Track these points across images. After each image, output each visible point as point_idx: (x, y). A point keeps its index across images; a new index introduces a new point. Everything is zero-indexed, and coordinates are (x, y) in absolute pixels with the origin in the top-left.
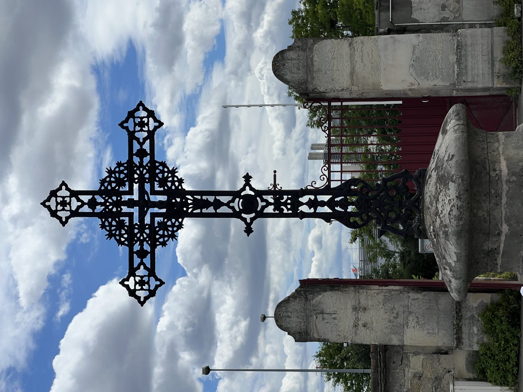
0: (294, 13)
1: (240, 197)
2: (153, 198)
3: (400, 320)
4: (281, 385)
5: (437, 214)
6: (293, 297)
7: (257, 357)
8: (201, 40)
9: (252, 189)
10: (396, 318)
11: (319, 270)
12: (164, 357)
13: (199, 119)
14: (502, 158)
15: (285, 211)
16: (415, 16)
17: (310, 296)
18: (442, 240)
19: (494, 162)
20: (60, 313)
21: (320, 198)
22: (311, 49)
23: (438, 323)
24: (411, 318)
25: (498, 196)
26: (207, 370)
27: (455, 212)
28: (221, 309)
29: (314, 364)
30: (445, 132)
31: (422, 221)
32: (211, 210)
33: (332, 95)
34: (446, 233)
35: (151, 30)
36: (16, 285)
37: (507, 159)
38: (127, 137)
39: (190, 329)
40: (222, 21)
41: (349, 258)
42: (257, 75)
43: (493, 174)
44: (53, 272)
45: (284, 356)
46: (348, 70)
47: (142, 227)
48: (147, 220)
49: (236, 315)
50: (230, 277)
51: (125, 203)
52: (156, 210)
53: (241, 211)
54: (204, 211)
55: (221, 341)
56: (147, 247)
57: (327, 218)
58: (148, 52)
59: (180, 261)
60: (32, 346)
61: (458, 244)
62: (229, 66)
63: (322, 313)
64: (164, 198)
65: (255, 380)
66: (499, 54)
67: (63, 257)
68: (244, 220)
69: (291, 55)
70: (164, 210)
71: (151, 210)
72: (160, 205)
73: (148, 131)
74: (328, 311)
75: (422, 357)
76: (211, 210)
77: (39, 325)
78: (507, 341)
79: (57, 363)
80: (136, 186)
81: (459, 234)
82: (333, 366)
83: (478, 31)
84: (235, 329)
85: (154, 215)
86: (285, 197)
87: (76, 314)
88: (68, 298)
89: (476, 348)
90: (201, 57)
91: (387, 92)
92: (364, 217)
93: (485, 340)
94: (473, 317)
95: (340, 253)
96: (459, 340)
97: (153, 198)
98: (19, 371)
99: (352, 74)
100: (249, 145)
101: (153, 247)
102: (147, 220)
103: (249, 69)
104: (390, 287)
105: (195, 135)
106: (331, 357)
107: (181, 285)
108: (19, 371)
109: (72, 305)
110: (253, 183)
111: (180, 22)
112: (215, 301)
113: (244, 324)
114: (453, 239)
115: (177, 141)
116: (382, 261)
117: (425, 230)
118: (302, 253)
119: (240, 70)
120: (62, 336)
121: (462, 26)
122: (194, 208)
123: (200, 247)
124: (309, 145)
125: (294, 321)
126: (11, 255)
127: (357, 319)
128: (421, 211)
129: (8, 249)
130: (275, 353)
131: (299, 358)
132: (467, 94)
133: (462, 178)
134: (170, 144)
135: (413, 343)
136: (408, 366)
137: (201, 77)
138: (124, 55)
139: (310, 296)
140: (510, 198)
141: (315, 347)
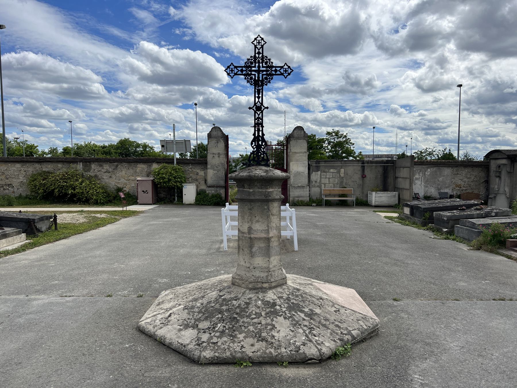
0: (315, 135)
1: (261, 105)
2: (261, 75)
3: (216, 168)
4: (192, 131)
5: (256, 170)
6: (223, 133)
7: (201, 123)
8: (308, 104)
9: (264, 109)
10: (216, 167)
11: (231, 144)
12: (201, 90)
13: (281, 104)
14: (273, 190)
15: (256, 121)
16: (314, 173)
17: (223, 138)
18: (247, 171)
19: (272, 187)
20: (216, 53)
21: (261, 132)
22: (304, 139)
23: (215, 180)
24: (216, 172)
25: (262, 188)
26: (196, 104)
27: (257, 175)
28: (217, 111)
29: (199, 142)
30: (282, 172)
31: (253, 165)
32: (257, 95)
33: (289, 146)
34: (250, 172)
35: (312, 87)
36: (226, 37)
37: (273, 191)
38: (282, 66)
39: (210, 100)
40: (314, 111)
41: (235, 154)
42: (295, 124)
43: (268, 187)
44: (230, 51)
45: (201, 132)
46: (297, 151)
47: (251, 71)
48: (253, 73)
49: (216, 116)
50: (228, 114)
51: (259, 65)
52: (257, 76)
53: (256, 106)
54: (257, 93)
55: (206, 111)
56: (244, 72)
57: (254, 135)
58: (305, 86)
59: (234, 96)
60: (204, 43)
61: (246, 176)
62: (298, 114)
63: (217, 143)
64: (261, 79)
65: (193, 122)
66: (300, 199)
67: (235, 54)
68: (253, 107)
69: (303, 132)
70: (257, 79)
71: (257, 74)
72: (259, 77)
73: (283, 73)
74: (218, 144)
75: (204, 175)
76: (257, 95)
77: (212, 45)
78: (210, 201)
79: (199, 52)
80: (265, 69)
81: (249, 176)
82: (199, 148)
83: (308, 193)
84: (211, 116)
85: (255, 75)
86: (261, 121)
87: (215, 59)
88: (221, 56)
89: (207, 192)
90: (302, 104)
91: (289, 164)
92: (254, 147)
93: (210, 195)
94: (217, 191)
95: (236, 151)
96: (210, 187)
97: (261, 75)
98: (195, 38)
99: (296, 153)
100: (272, 121)
101: (255, 56)
102: (253, 73)
103: (297, 121)
104: (226, 165)
105: (276, 102)
106: (202, 147)
107: (226, 97)
108: (195, 38)
109: (219, 57)
110: (266, 109)
111: (314, 97)
112: (220, 109)
113: (212, 119)
114: (248, 174)
115: (274, 96)
116: (234, 164)
117: (250, 166)
118: (236, 139)
119: (297, 118)
120: (208, 54)
121: (310, 188)
122: (257, 89)
123: (238, 104)
124: (271, 141)
125: (214, 133)
126: (236, 36)
127: (215, 154)
128: (256, 165)
129: (238, 35)
130: (203, 129)
131: (201, 137)
132: (288, 189)
133: (267, 177)
134: (273, 93)
135: (208, 172)
136: (201, 171)
137: (296, 104)
138: (304, 77)
139: (223, 138)
140: (261, 192)
141: (205, 142)
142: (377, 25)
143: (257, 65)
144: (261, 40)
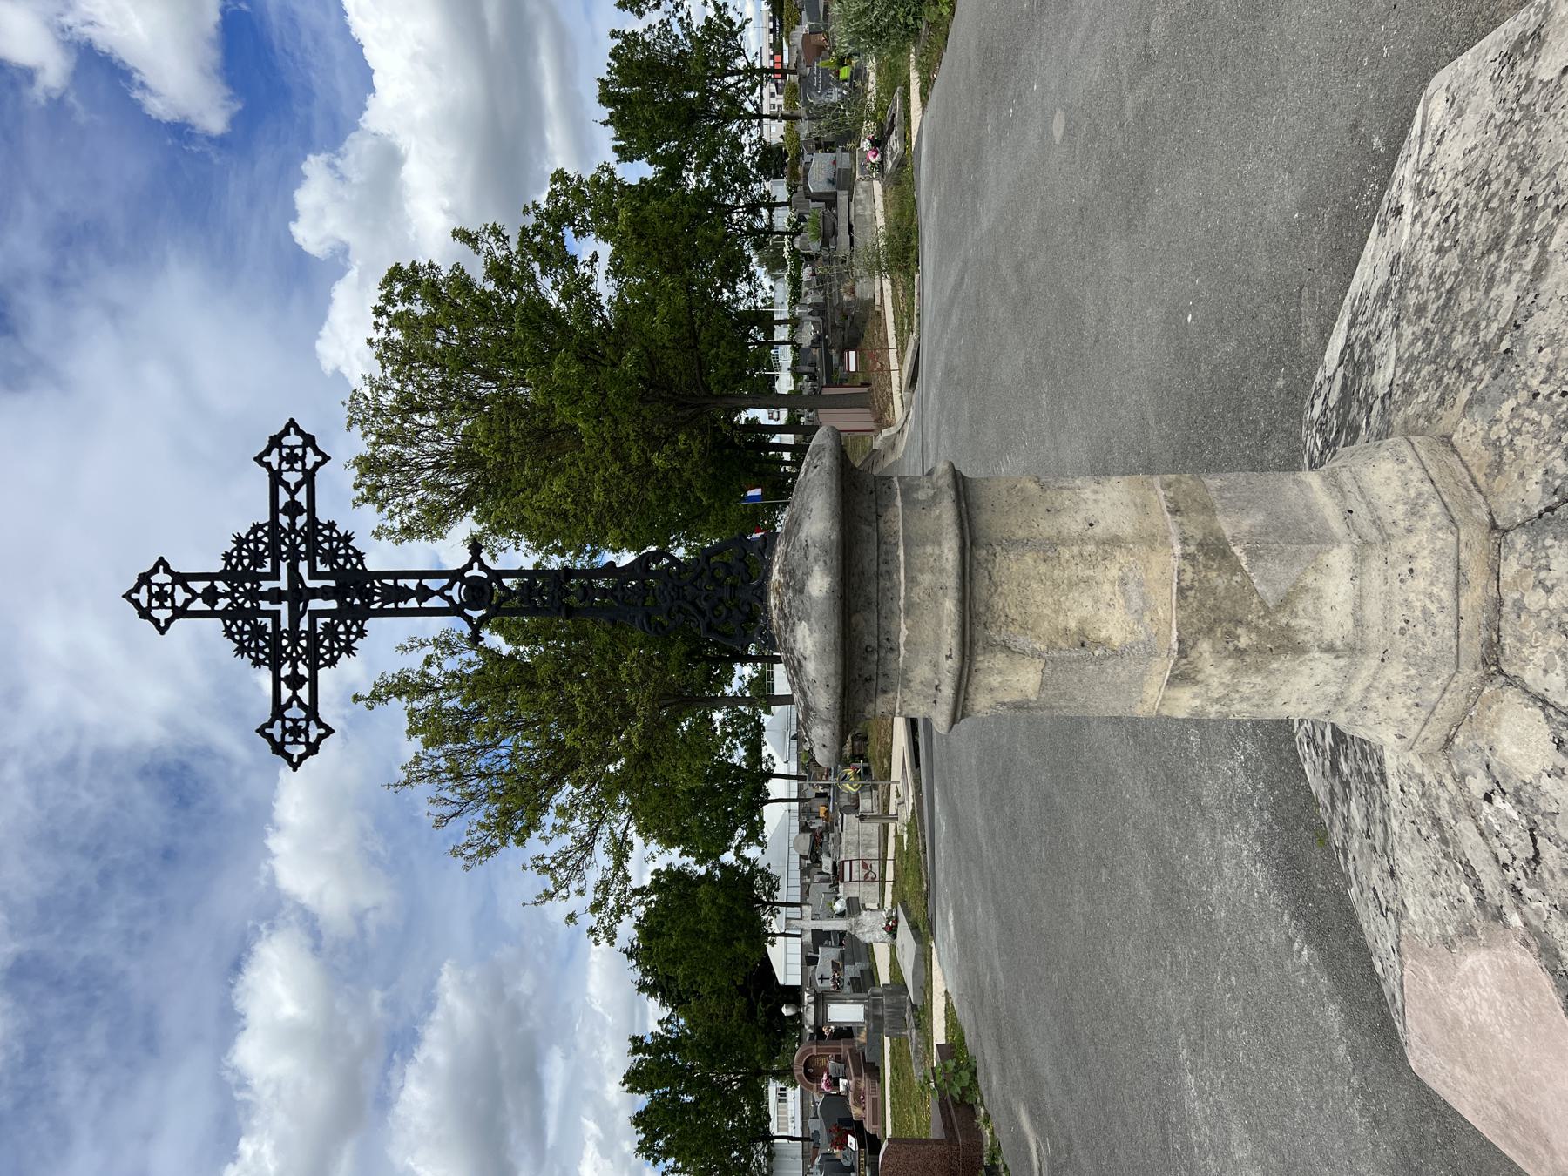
143: (265, 605)
144: (150, 584)
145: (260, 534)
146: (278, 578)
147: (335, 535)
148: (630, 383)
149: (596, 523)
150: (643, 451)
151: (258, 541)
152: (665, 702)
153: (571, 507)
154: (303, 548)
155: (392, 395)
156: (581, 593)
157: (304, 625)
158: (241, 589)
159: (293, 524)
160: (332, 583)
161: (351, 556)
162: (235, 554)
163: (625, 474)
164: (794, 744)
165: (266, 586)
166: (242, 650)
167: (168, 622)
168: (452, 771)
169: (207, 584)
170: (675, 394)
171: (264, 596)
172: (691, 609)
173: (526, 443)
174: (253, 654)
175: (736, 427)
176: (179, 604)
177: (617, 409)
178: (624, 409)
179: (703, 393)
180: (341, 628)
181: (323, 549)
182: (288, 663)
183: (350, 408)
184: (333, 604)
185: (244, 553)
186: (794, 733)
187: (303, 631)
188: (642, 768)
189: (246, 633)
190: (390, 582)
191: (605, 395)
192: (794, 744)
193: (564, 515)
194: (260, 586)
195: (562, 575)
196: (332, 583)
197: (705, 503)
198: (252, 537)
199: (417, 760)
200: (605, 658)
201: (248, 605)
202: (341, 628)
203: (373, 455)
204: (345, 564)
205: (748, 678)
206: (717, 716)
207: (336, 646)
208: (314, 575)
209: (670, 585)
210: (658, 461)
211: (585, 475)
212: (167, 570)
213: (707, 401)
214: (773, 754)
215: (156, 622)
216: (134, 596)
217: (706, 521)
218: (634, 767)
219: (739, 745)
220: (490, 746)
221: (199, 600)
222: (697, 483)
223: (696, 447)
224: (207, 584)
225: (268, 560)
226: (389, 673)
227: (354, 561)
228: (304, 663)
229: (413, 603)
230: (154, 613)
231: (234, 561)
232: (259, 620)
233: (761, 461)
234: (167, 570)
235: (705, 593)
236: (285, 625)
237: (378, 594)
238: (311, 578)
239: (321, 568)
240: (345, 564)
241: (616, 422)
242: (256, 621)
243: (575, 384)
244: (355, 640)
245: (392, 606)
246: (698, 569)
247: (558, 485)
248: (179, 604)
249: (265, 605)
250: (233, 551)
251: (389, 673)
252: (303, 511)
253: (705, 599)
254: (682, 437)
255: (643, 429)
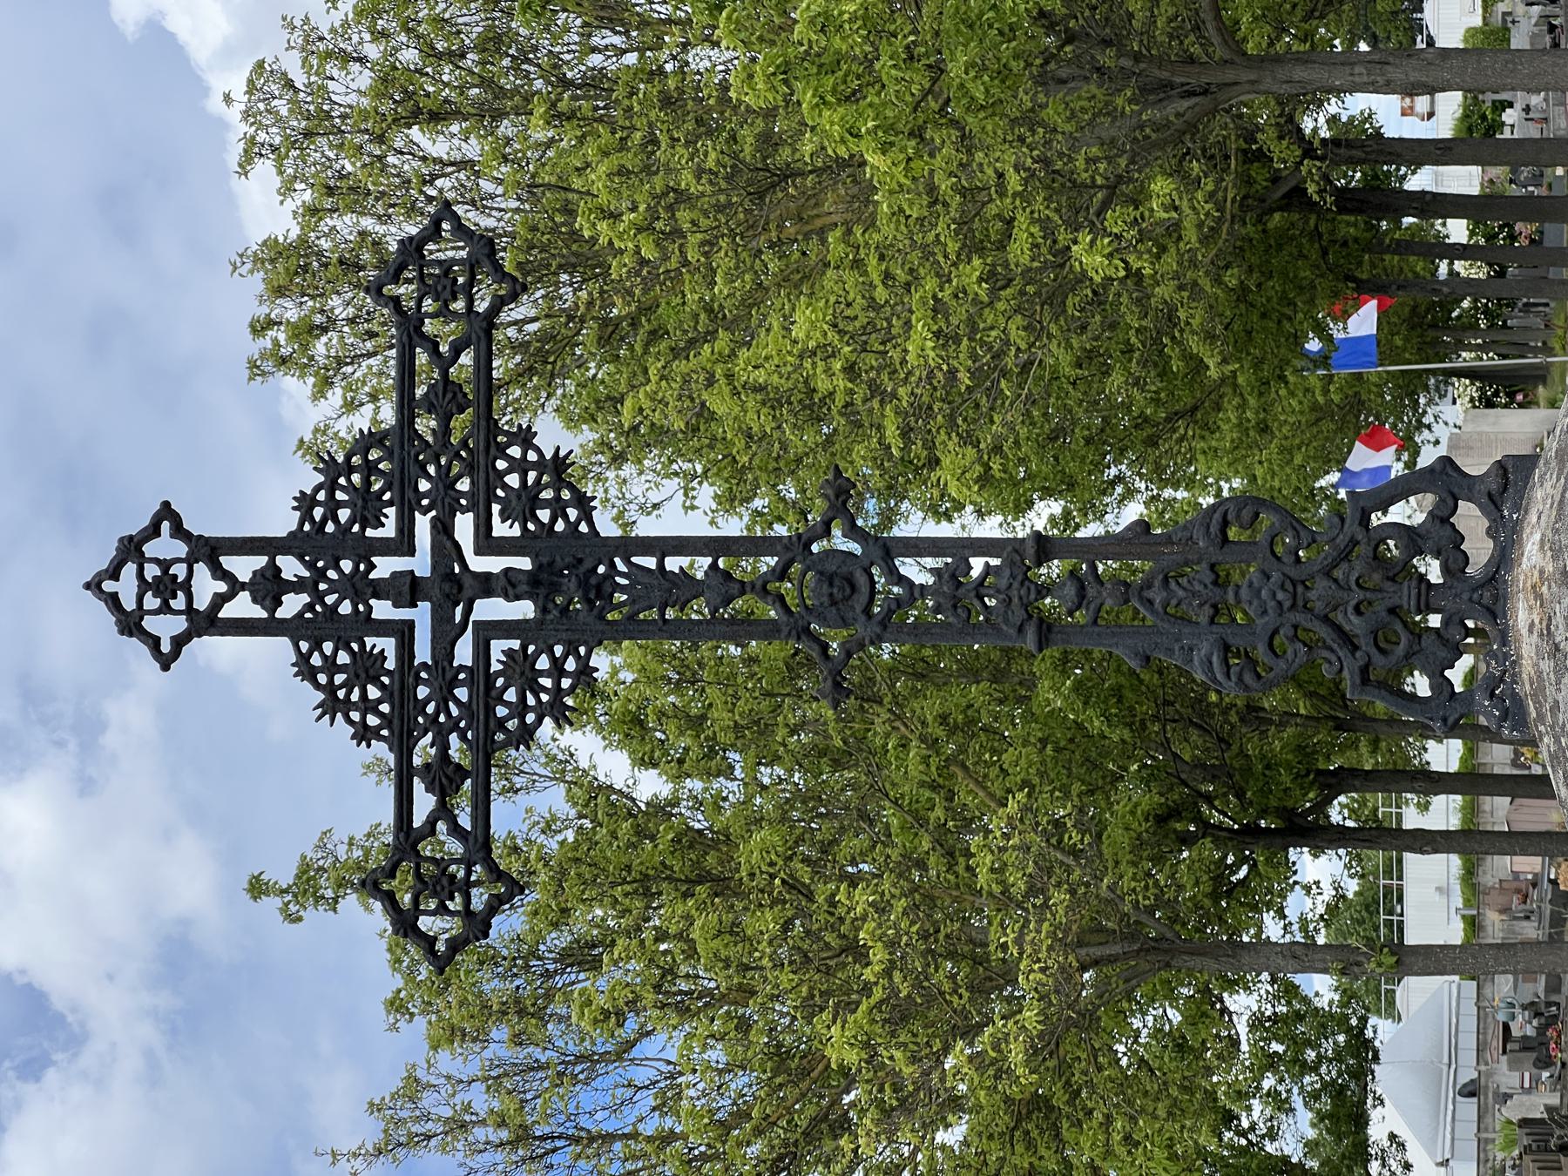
142: (265, 243)
143: (382, 609)
144: (141, 560)
145: (374, 455)
146: (411, 552)
147: (532, 456)
148: (1009, 33)
149: (906, 433)
150: (1048, 230)
151: (370, 469)
152: (1097, 952)
153: (841, 383)
154: (464, 485)
155: (363, 78)
156: (1070, 591)
157: (464, 653)
158: (332, 574)
159: (444, 431)
160: (524, 563)
161: (567, 504)
162: (321, 496)
163: (994, 292)
164: (1469, 1107)
165: (385, 566)
166: (332, 706)
167: (179, 642)
168: (502, 1124)
169: (260, 561)
170: (1137, 57)
171: (379, 590)
172: (1324, 632)
173: (720, 208)
174: (355, 716)
175: (1308, 148)
176: (201, 603)
177: (973, 106)
178: (992, 107)
179: (1220, 52)
180: (543, 663)
181: (505, 487)
182: (430, 736)
183: (246, 114)
184: (524, 609)
185: (340, 496)
186: (1468, 1075)
187: (462, 668)
188: (1030, 1145)
189: (341, 669)
190: (650, 562)
191: (937, 70)
192: (1469, 1107)
193: (813, 407)
194: (372, 567)
195: (1030, 550)
196: (524, 563)
197: (1213, 373)
198: (356, 460)
199: (413, 1087)
200: (922, 821)
201: (345, 608)
202: (543, 663)
203: (303, 240)
204: (553, 520)
205: (1328, 894)
206: (1242, 1004)
207: (531, 701)
208: (487, 543)
209: (1276, 576)
210: (1090, 258)
211: (881, 294)
212: (179, 531)
213: (1229, 75)
214: (1404, 1134)
215: (154, 642)
216: (108, 586)
217: (1210, 429)
218: (1008, 1137)
219: (1297, 1101)
220: (605, 1057)
221: (244, 596)
222: (1193, 316)
223: (1196, 211)
224: (260, 561)
225: (391, 511)
226: (341, 835)
227: (573, 513)
228: (463, 738)
229: (698, 610)
230: (149, 623)
231: (318, 513)
232: (369, 641)
233: (1376, 245)
234: (179, 531)
235: (1358, 595)
236: (423, 652)
237: (623, 589)
238: (478, 552)
239: (501, 529)
240: (553, 520)
241: (966, 142)
242: (363, 645)
243: (854, 42)
244: (350, 722)
245: (654, 614)
246: (1342, 540)
247: (807, 322)
248: (201, 603)
249: (382, 609)
250: (317, 489)
251: (341, 835)
252: (468, 404)
253: (1358, 610)
254: (1161, 186)
255: (1044, 161)
